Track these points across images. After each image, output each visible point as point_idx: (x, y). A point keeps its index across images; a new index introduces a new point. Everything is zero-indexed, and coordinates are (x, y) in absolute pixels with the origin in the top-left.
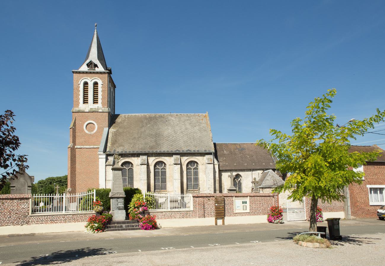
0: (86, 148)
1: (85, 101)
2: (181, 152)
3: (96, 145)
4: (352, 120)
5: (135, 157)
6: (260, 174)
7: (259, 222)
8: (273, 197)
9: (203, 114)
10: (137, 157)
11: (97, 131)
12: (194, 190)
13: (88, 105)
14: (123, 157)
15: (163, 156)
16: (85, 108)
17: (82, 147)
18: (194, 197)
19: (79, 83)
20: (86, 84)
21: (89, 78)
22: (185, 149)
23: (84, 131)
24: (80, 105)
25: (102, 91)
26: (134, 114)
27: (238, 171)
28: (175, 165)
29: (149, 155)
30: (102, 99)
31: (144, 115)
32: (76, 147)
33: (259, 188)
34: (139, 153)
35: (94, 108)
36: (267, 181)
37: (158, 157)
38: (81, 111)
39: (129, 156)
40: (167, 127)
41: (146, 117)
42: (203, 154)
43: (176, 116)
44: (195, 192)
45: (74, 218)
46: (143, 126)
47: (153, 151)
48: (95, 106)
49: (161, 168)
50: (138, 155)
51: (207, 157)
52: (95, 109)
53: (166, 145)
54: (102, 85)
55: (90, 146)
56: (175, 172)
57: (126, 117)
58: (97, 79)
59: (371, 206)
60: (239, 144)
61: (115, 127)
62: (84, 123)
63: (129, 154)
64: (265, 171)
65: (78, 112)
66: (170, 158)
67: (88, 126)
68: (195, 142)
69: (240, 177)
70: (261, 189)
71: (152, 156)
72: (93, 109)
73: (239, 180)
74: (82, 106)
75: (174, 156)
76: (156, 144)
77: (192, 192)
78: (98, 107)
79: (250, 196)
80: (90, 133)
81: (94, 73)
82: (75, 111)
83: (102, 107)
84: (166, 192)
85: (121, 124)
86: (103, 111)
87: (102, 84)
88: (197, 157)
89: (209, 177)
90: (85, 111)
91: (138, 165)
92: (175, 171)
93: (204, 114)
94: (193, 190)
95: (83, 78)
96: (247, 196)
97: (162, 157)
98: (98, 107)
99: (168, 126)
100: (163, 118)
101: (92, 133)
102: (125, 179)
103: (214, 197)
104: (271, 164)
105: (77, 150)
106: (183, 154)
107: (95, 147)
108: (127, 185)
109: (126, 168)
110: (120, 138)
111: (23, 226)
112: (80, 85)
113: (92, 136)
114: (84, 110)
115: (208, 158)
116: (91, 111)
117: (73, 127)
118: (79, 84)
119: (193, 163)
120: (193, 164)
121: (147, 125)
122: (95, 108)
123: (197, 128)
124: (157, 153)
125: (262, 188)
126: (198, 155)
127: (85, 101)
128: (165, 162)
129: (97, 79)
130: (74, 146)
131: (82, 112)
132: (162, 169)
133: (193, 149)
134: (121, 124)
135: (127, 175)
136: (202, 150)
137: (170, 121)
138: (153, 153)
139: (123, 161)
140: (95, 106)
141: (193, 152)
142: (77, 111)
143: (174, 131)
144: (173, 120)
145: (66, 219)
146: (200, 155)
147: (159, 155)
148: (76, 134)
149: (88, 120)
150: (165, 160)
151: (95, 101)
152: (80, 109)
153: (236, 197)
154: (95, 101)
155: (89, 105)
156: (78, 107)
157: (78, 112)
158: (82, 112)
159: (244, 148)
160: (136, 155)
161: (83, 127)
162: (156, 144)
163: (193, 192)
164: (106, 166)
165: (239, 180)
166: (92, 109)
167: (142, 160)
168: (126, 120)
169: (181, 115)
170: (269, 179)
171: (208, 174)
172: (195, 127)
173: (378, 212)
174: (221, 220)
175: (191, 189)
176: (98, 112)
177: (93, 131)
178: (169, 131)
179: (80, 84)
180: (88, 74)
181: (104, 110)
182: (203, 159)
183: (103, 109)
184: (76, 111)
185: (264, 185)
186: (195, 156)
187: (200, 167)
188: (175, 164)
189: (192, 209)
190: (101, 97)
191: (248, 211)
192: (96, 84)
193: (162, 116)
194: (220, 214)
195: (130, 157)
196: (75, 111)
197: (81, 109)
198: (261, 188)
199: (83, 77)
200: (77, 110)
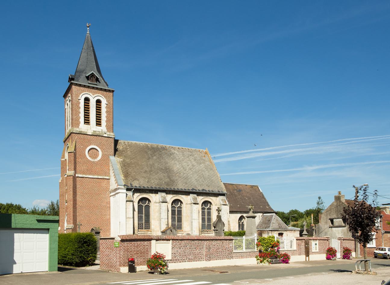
0: (89, 178)
1: (87, 121)
2: (198, 191)
3: (100, 175)
4: (366, 184)
5: (153, 193)
6: (260, 217)
7: (199, 267)
8: (328, 240)
9: (204, 150)
10: (155, 193)
11: (101, 158)
12: (208, 230)
13: (91, 127)
14: (140, 193)
15: (180, 194)
16: (88, 130)
17: (85, 176)
18: (297, 240)
19: (80, 98)
20: (87, 100)
21: (91, 94)
22: (199, 188)
23: (86, 157)
24: (80, 124)
25: (107, 112)
26: (135, 142)
27: (242, 213)
28: (194, 205)
29: (168, 192)
30: (106, 121)
31: (145, 144)
32: (77, 175)
33: (269, 230)
34: (157, 189)
35: (98, 131)
36: (274, 224)
37: (176, 195)
38: (82, 133)
39: (147, 191)
40: (173, 161)
41: (148, 146)
42: (216, 195)
43: (178, 150)
44: (209, 232)
45: (248, 255)
46: (150, 158)
47: (170, 188)
48: (98, 129)
49: (145, 205)
50: (156, 191)
51: (221, 197)
52: (98, 133)
53: (180, 182)
54: (107, 104)
55: (93, 175)
56: (195, 211)
57: (126, 144)
58: (101, 97)
59: (368, 248)
60: (236, 185)
61: (119, 155)
62: (86, 148)
63: (147, 190)
64: (264, 214)
65: (79, 134)
66: (186, 196)
67: (92, 150)
68: (207, 182)
69: (243, 219)
70: (270, 232)
71: (170, 194)
72: (97, 132)
73: (242, 221)
74: (83, 127)
75: (191, 195)
76: (170, 180)
77: (206, 232)
78: (102, 130)
79: (319, 240)
80: (93, 160)
81: (97, 89)
82: (76, 131)
83: (106, 130)
84: (183, 232)
85: (124, 152)
86: (109, 136)
87: (107, 103)
88: (211, 198)
89: (224, 218)
90: (88, 134)
91: (156, 202)
92: (194, 210)
93: (205, 151)
94: (206, 230)
95: (85, 93)
96: (317, 240)
97: (179, 195)
98: (102, 130)
99: (175, 161)
100: (166, 150)
101: (96, 160)
102: (141, 217)
103: (304, 240)
104: (267, 207)
105: (77, 179)
106: (199, 194)
107: (100, 177)
108: (143, 223)
109: (143, 205)
110: (130, 170)
111: (211, 261)
112: (80, 100)
113: (96, 163)
114: (86, 132)
115: (222, 198)
116: (95, 134)
117: (75, 152)
118: (79, 99)
119: (206, 203)
120: (206, 204)
121: (152, 157)
122: (99, 132)
123: (202, 165)
124: (175, 191)
125: (271, 231)
126: (212, 195)
127: (87, 121)
128: (182, 200)
129: (101, 97)
130: (75, 175)
131: (84, 134)
132: (178, 207)
133: (208, 189)
134: (124, 152)
135: (143, 212)
136: (216, 190)
137: (174, 154)
138: (171, 191)
139: (141, 197)
140: (98, 129)
141: (208, 192)
142: (78, 132)
143: (182, 166)
144: (177, 154)
145: (242, 255)
146: (213, 195)
147: (176, 193)
148: (77, 159)
149: (90, 145)
150: (182, 198)
151: (99, 123)
152: (81, 130)
153: (313, 240)
154: (99, 123)
155: (92, 127)
156: (78, 127)
157: (79, 134)
158: (84, 134)
159: (241, 189)
160: (154, 192)
161: (85, 152)
162: (170, 180)
163: (207, 233)
164: (127, 201)
165: (242, 222)
166: (95, 131)
167: (162, 198)
168: (128, 148)
169: (182, 148)
170: (275, 222)
171: (223, 215)
172: (201, 164)
173: (375, 252)
174: (308, 257)
175: (204, 229)
176: (102, 136)
177: (96, 158)
178: (178, 166)
179: (80, 99)
180: (90, 88)
181: (109, 135)
182: (216, 200)
183: (108, 133)
184: (77, 132)
185: (272, 228)
186: (210, 196)
187: (184, 206)
188: (194, 204)
189: (295, 249)
190: (106, 118)
191: (317, 251)
192: (98, 102)
193: (164, 148)
194: (307, 254)
195: (147, 193)
196: (75, 132)
197: (83, 130)
198: (270, 230)
199: (83, 91)
200: (77, 131)
